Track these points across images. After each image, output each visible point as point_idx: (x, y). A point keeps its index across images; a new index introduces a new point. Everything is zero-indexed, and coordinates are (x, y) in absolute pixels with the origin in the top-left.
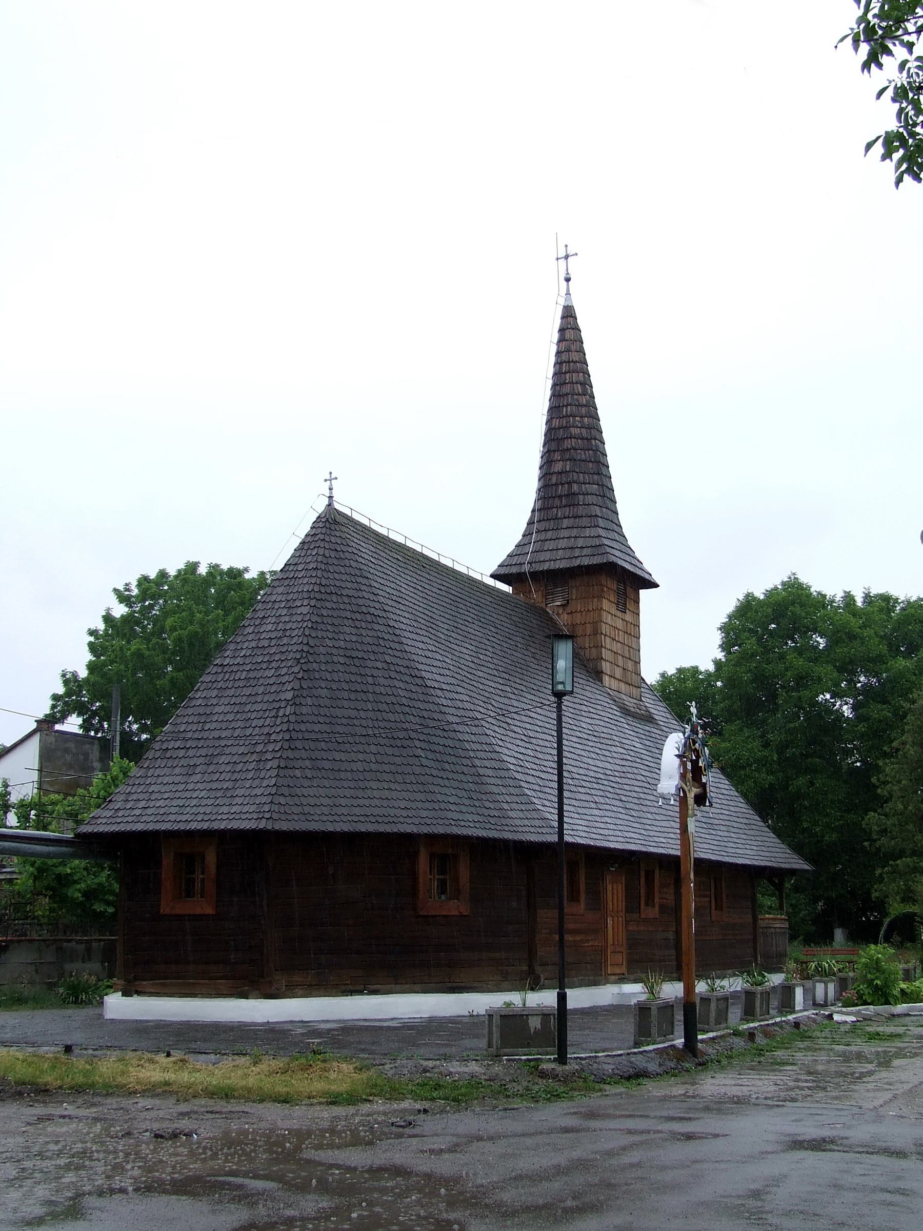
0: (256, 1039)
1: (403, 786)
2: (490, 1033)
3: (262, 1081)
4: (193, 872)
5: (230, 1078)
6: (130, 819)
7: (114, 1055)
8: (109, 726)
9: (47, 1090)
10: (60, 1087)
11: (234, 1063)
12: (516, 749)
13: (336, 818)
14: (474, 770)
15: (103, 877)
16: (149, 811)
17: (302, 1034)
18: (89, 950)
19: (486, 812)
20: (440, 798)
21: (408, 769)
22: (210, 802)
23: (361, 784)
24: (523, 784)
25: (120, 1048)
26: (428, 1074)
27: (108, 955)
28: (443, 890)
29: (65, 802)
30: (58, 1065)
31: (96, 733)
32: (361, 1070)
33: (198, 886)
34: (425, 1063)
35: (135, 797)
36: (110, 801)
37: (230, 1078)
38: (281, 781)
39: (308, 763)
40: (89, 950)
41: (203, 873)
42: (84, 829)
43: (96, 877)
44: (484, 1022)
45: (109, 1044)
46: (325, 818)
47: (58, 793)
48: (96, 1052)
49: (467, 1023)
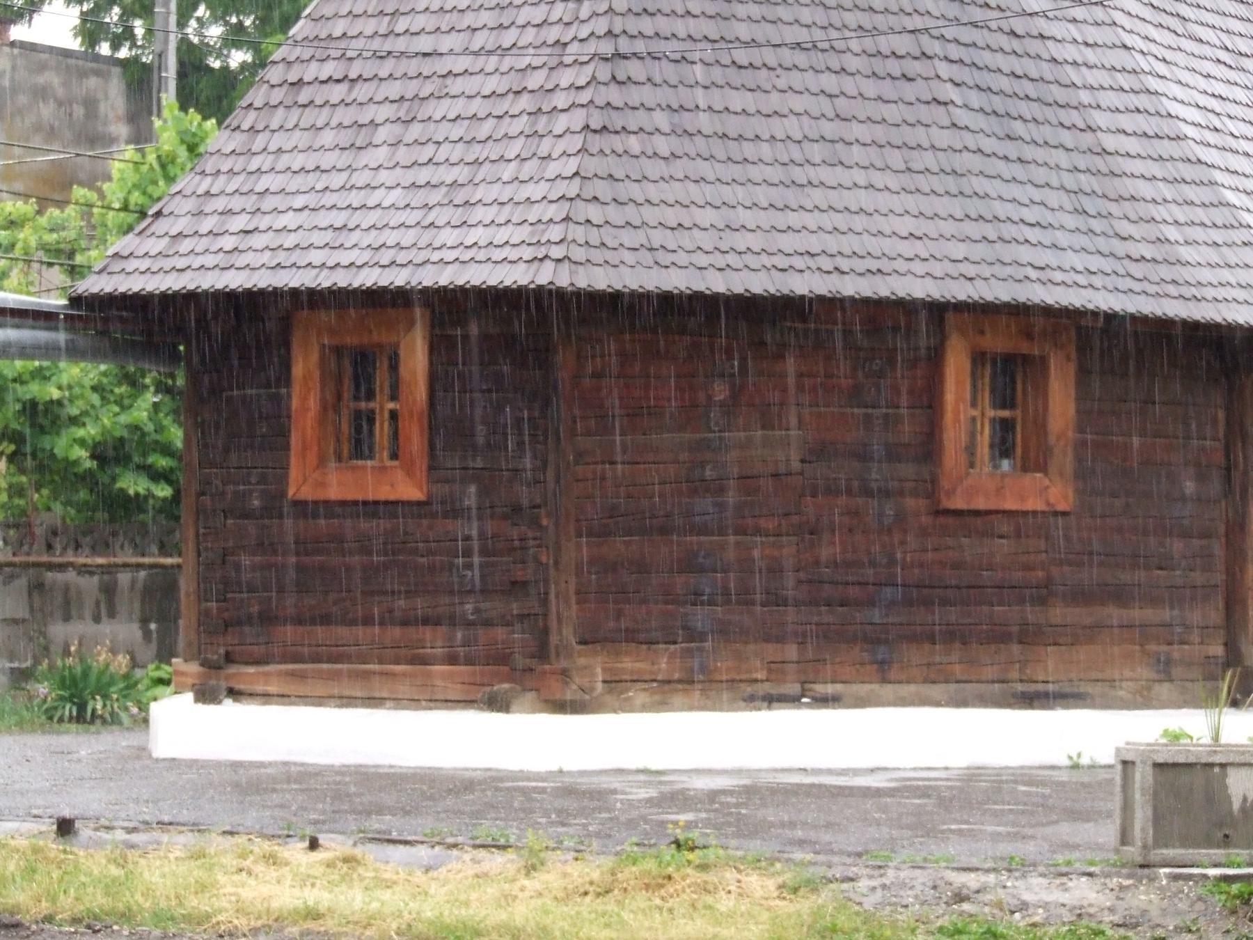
0: (532, 811)
1: (905, 180)
2: (1127, 807)
3: (547, 912)
4: (370, 395)
5: (467, 904)
6: (209, 260)
7: (180, 842)
8: (149, 32)
9: (17, 925)
10: (49, 919)
11: (478, 869)
12: (1202, 83)
13: (732, 259)
14: (1089, 136)
15: (142, 410)
16: (258, 241)
17: (649, 801)
18: (109, 591)
19: (1121, 248)
20: (1002, 210)
21: (920, 135)
22: (412, 217)
23: (799, 174)
24: (1219, 176)
25: (197, 828)
26: (966, 906)
27: (159, 601)
28: (1003, 448)
29: (43, 221)
30: (41, 867)
31: (116, 47)
32: (795, 890)
33: (382, 430)
34: (959, 879)
35: (220, 204)
36: (159, 214)
37: (467, 904)
38: (592, 165)
39: (661, 120)
40: (109, 591)
41: (394, 397)
42: (93, 285)
43: (124, 408)
44: (1110, 782)
45: (166, 819)
46: (703, 260)
47: (26, 196)
48: (135, 838)
49: (1062, 784)
